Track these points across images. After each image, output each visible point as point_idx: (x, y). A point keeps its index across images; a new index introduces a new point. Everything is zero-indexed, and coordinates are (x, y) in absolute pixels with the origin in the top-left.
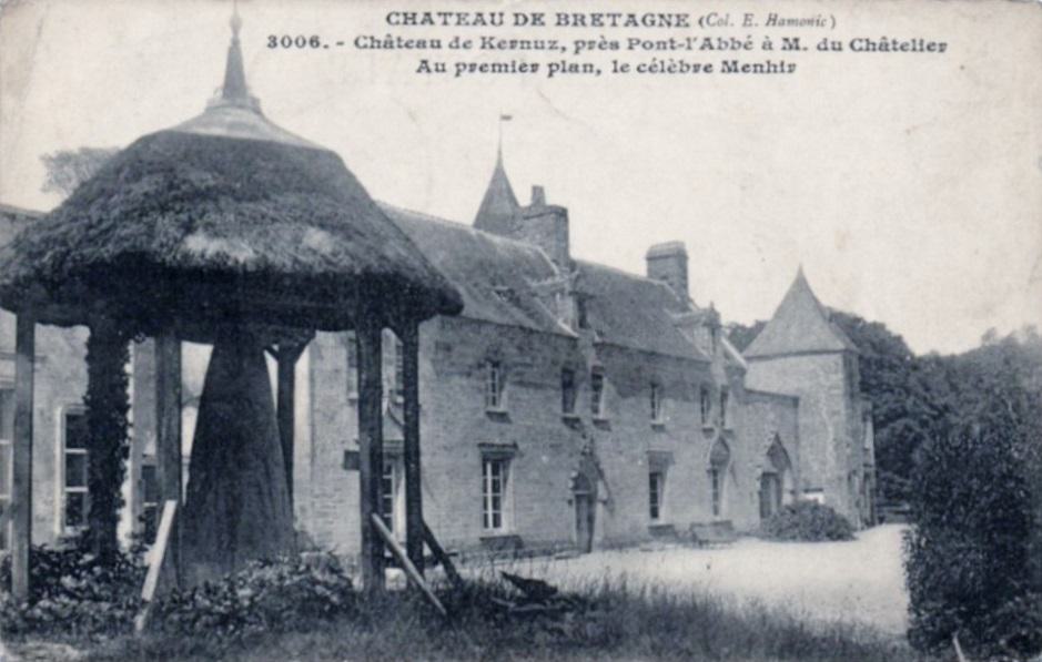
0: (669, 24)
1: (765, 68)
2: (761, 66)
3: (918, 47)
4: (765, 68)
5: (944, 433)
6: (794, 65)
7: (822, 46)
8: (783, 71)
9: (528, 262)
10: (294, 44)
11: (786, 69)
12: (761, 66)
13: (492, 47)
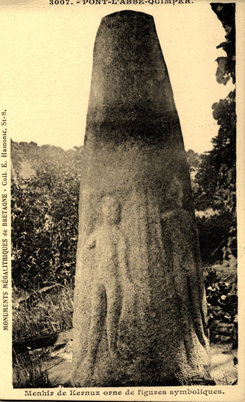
0: (163, 392)
1: (208, 392)
2: (40, 393)
3: (200, 392)
4: (208, 392)
5: (97, 366)
6: (53, 393)
7: (127, 393)
8: (48, 395)
9: (124, 110)
10: (192, 393)
11: (50, 394)
12: (40, 393)
13: (74, 394)
